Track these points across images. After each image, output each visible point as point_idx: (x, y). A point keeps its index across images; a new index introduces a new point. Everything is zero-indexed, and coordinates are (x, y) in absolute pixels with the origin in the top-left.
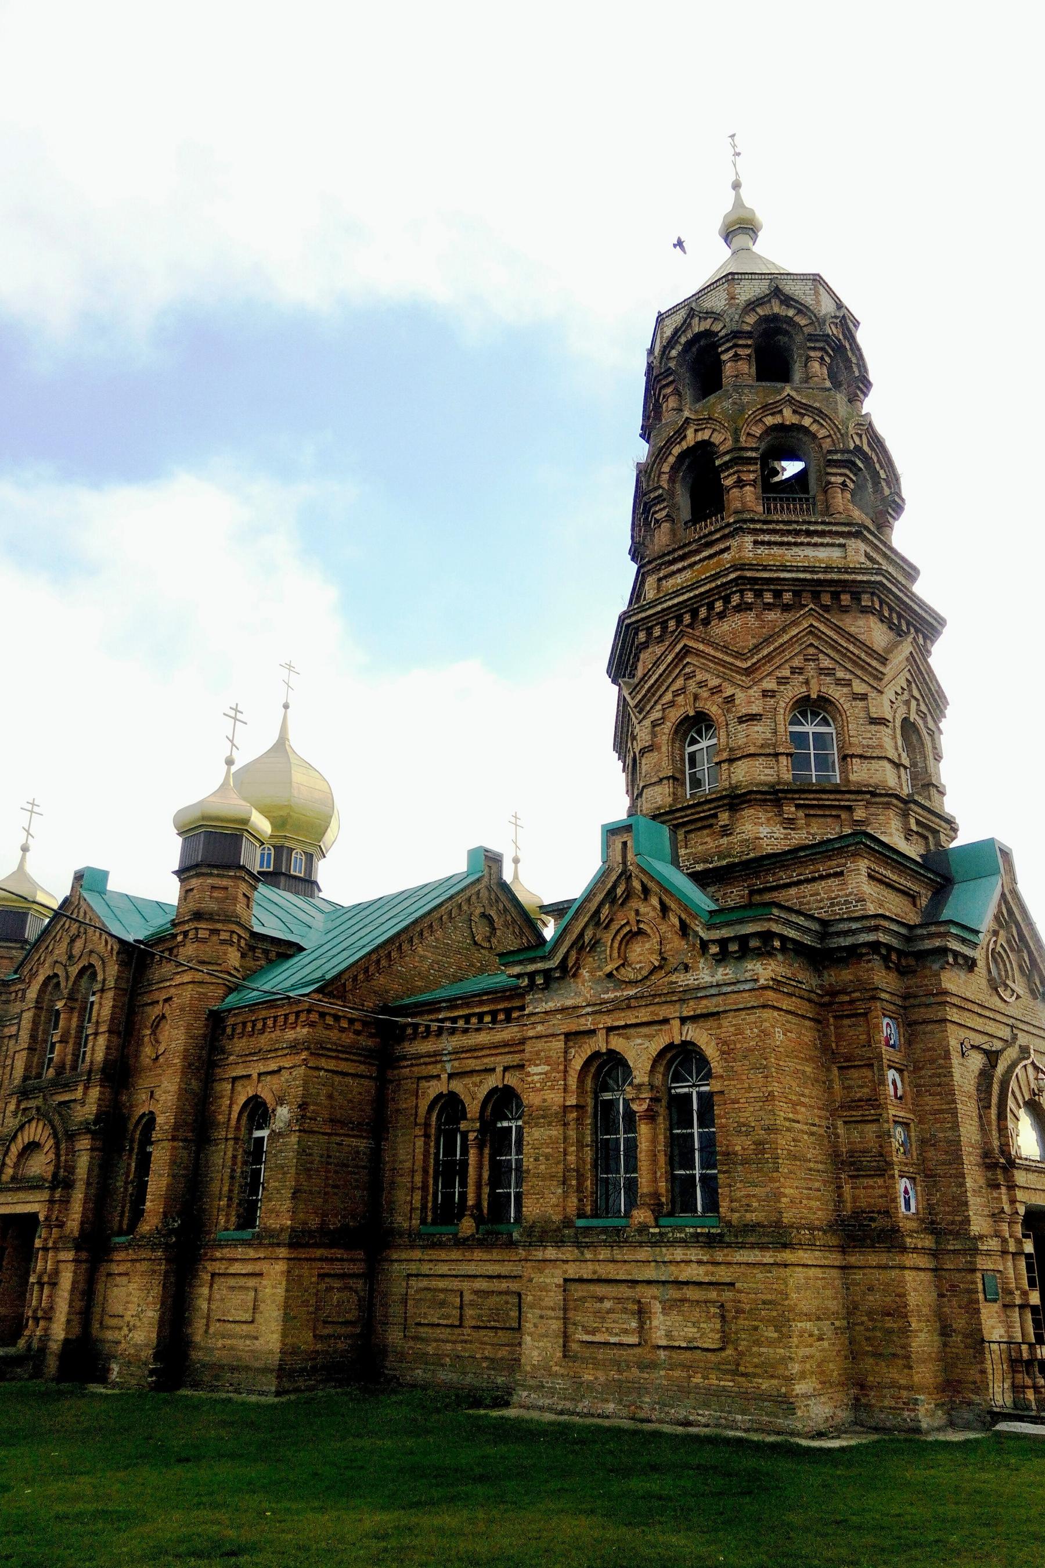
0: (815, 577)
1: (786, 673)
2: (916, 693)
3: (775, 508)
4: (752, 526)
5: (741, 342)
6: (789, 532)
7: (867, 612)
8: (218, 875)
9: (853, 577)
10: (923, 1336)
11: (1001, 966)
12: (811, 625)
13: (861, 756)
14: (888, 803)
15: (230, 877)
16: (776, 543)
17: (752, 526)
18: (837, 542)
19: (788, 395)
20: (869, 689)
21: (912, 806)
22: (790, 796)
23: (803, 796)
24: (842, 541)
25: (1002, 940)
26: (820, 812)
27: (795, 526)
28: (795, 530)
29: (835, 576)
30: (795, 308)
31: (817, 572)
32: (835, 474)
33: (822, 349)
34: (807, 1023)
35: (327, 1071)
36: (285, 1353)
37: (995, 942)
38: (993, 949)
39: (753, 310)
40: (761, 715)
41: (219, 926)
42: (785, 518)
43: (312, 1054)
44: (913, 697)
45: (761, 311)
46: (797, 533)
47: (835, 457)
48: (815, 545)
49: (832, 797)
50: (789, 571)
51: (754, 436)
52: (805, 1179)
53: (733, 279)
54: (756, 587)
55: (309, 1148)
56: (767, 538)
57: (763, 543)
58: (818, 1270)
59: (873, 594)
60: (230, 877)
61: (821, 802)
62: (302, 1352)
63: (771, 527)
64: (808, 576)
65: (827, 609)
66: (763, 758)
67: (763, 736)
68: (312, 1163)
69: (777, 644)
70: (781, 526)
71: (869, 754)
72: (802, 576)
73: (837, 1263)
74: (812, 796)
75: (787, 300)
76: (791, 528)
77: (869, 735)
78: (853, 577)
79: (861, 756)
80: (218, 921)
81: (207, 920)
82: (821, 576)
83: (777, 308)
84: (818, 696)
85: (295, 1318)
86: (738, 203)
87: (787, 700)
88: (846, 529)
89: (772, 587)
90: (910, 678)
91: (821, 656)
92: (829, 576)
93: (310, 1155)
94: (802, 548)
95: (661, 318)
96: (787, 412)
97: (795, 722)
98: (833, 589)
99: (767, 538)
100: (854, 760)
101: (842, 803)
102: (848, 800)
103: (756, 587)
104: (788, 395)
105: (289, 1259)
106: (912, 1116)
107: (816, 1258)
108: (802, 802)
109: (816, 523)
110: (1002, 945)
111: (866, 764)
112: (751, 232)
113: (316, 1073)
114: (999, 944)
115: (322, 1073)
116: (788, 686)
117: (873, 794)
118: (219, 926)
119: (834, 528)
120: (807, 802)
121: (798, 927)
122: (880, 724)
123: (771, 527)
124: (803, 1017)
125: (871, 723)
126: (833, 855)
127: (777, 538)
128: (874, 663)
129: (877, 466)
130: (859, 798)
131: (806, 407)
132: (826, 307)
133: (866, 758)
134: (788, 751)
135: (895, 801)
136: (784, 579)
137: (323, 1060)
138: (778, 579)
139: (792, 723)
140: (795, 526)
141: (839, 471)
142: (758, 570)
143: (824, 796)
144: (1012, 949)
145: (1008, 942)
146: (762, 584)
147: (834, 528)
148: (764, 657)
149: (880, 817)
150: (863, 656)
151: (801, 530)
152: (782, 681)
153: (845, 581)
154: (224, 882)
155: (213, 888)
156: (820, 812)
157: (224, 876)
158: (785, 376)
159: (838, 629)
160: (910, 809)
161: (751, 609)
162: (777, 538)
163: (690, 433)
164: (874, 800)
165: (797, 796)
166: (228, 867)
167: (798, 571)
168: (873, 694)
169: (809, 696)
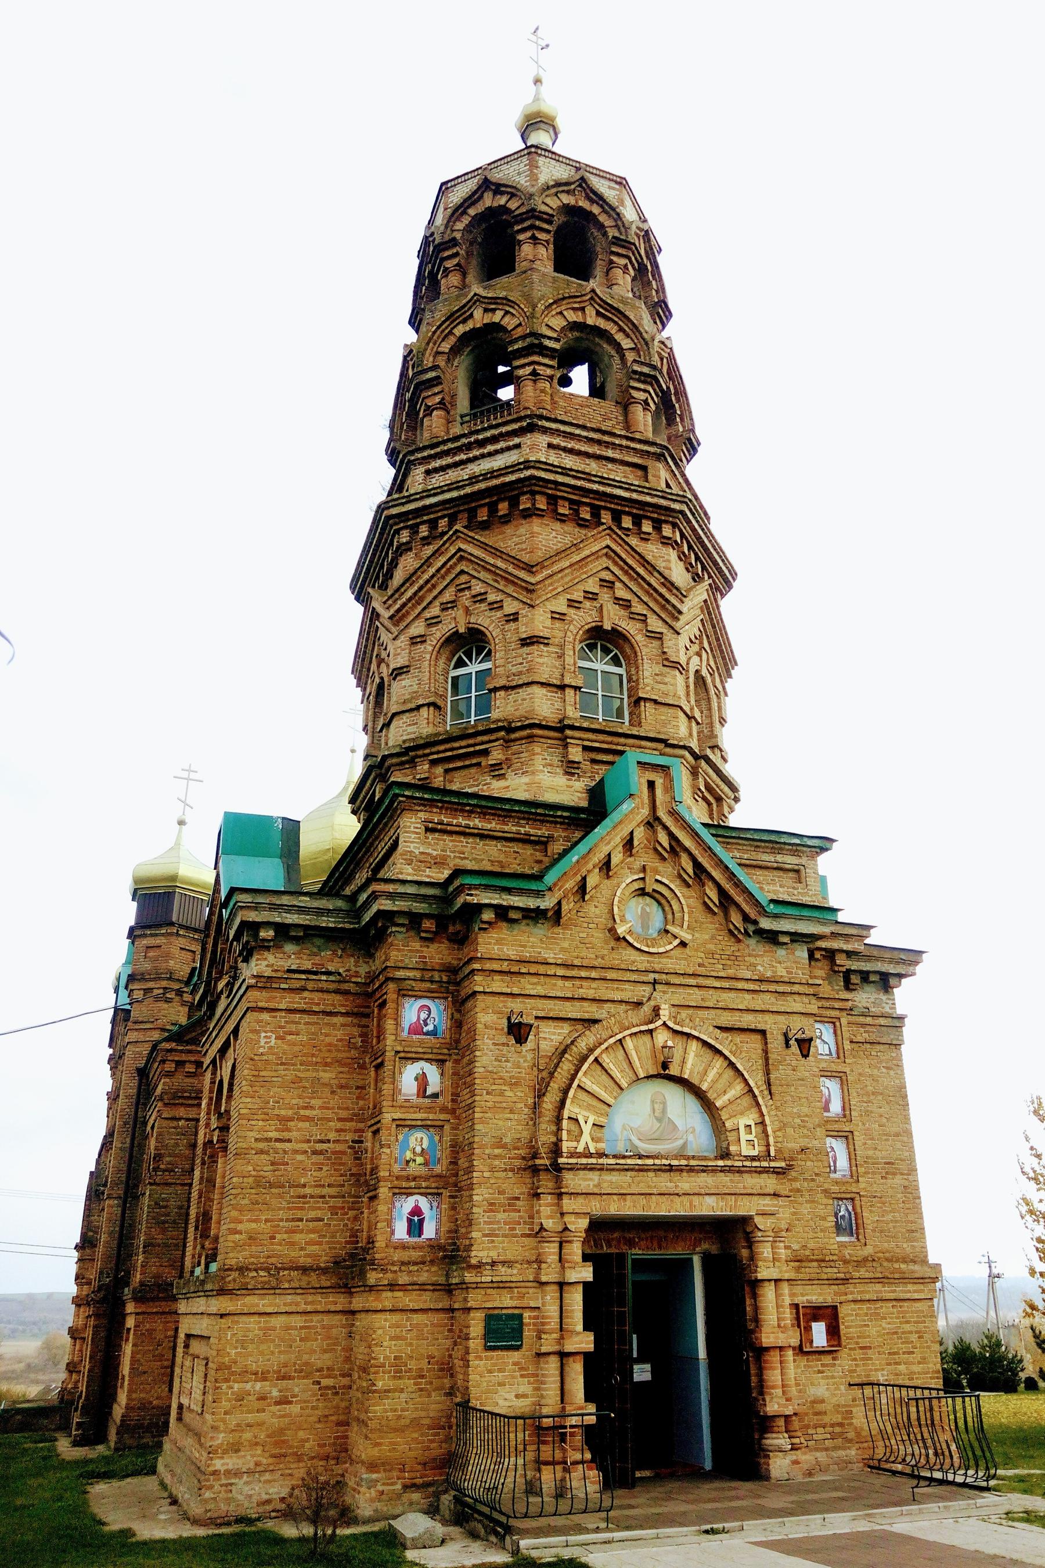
0: (462, 493)
1: (435, 610)
4: (419, 456)
5: (446, 254)
6: (459, 450)
7: (530, 516)
8: (152, 935)
9: (502, 480)
11: (667, 908)
12: (460, 550)
13: (505, 688)
14: (531, 737)
15: (163, 935)
16: (449, 466)
17: (419, 456)
18: (511, 443)
19: (475, 294)
20: (521, 606)
22: (420, 753)
23: (434, 750)
24: (517, 440)
26: (459, 764)
27: (465, 441)
28: (464, 445)
29: (482, 486)
30: (508, 193)
31: (463, 487)
32: (523, 366)
33: (532, 227)
34: (338, 1020)
35: (188, 1120)
40: (407, 667)
41: (151, 985)
43: (166, 1105)
45: (472, 212)
46: (469, 447)
47: (516, 347)
48: (490, 454)
49: (463, 743)
50: (435, 495)
51: (443, 353)
52: (289, 1209)
53: (447, 188)
54: (410, 523)
55: (163, 1200)
56: (437, 463)
57: (436, 470)
58: (298, 1318)
59: (533, 493)
60: (163, 935)
61: (455, 753)
62: (153, 1408)
63: (438, 450)
64: (455, 494)
65: (485, 526)
66: (407, 714)
67: (410, 690)
68: (168, 1215)
69: (421, 582)
70: (450, 445)
71: (514, 683)
72: (448, 496)
73: (339, 1307)
74: (442, 748)
75: (498, 188)
76: (459, 444)
77: (520, 660)
78: (502, 480)
79: (505, 688)
80: (151, 980)
81: (139, 980)
82: (468, 490)
83: (488, 201)
84: (469, 629)
85: (145, 1373)
86: (537, 99)
87: (434, 643)
88: (516, 426)
89: (425, 518)
92: (476, 487)
93: (165, 1207)
94: (477, 462)
96: (590, 311)
98: (487, 500)
99: (437, 463)
100: (498, 694)
101: (478, 748)
102: (483, 743)
103: (410, 523)
104: (475, 294)
105: (137, 1314)
106: (442, 1117)
107: (285, 1304)
108: (435, 756)
109: (484, 429)
111: (513, 695)
112: (542, 125)
113: (175, 1124)
115: (181, 1123)
116: (440, 625)
117: (510, 730)
118: (151, 985)
119: (504, 429)
120: (441, 755)
121: (301, 910)
122: (532, 644)
123: (438, 450)
125: (523, 645)
126: (803, 852)
127: (449, 460)
128: (522, 574)
130: (493, 738)
131: (494, 300)
133: (514, 688)
134: (427, 701)
136: (431, 506)
137: (182, 1109)
138: (425, 507)
140: (465, 441)
141: (526, 361)
142: (403, 504)
143: (456, 745)
146: (414, 518)
147: (504, 429)
148: (410, 600)
149: (522, 755)
150: (511, 569)
151: (470, 443)
152: (433, 622)
153: (496, 487)
154: (158, 941)
155: (149, 947)
156: (459, 764)
157: (156, 935)
158: (584, 274)
159: (484, 546)
160: (567, 737)
161: (410, 549)
162: (449, 460)
164: (513, 736)
165: (427, 751)
166: (159, 926)
167: (443, 492)
168: (524, 611)
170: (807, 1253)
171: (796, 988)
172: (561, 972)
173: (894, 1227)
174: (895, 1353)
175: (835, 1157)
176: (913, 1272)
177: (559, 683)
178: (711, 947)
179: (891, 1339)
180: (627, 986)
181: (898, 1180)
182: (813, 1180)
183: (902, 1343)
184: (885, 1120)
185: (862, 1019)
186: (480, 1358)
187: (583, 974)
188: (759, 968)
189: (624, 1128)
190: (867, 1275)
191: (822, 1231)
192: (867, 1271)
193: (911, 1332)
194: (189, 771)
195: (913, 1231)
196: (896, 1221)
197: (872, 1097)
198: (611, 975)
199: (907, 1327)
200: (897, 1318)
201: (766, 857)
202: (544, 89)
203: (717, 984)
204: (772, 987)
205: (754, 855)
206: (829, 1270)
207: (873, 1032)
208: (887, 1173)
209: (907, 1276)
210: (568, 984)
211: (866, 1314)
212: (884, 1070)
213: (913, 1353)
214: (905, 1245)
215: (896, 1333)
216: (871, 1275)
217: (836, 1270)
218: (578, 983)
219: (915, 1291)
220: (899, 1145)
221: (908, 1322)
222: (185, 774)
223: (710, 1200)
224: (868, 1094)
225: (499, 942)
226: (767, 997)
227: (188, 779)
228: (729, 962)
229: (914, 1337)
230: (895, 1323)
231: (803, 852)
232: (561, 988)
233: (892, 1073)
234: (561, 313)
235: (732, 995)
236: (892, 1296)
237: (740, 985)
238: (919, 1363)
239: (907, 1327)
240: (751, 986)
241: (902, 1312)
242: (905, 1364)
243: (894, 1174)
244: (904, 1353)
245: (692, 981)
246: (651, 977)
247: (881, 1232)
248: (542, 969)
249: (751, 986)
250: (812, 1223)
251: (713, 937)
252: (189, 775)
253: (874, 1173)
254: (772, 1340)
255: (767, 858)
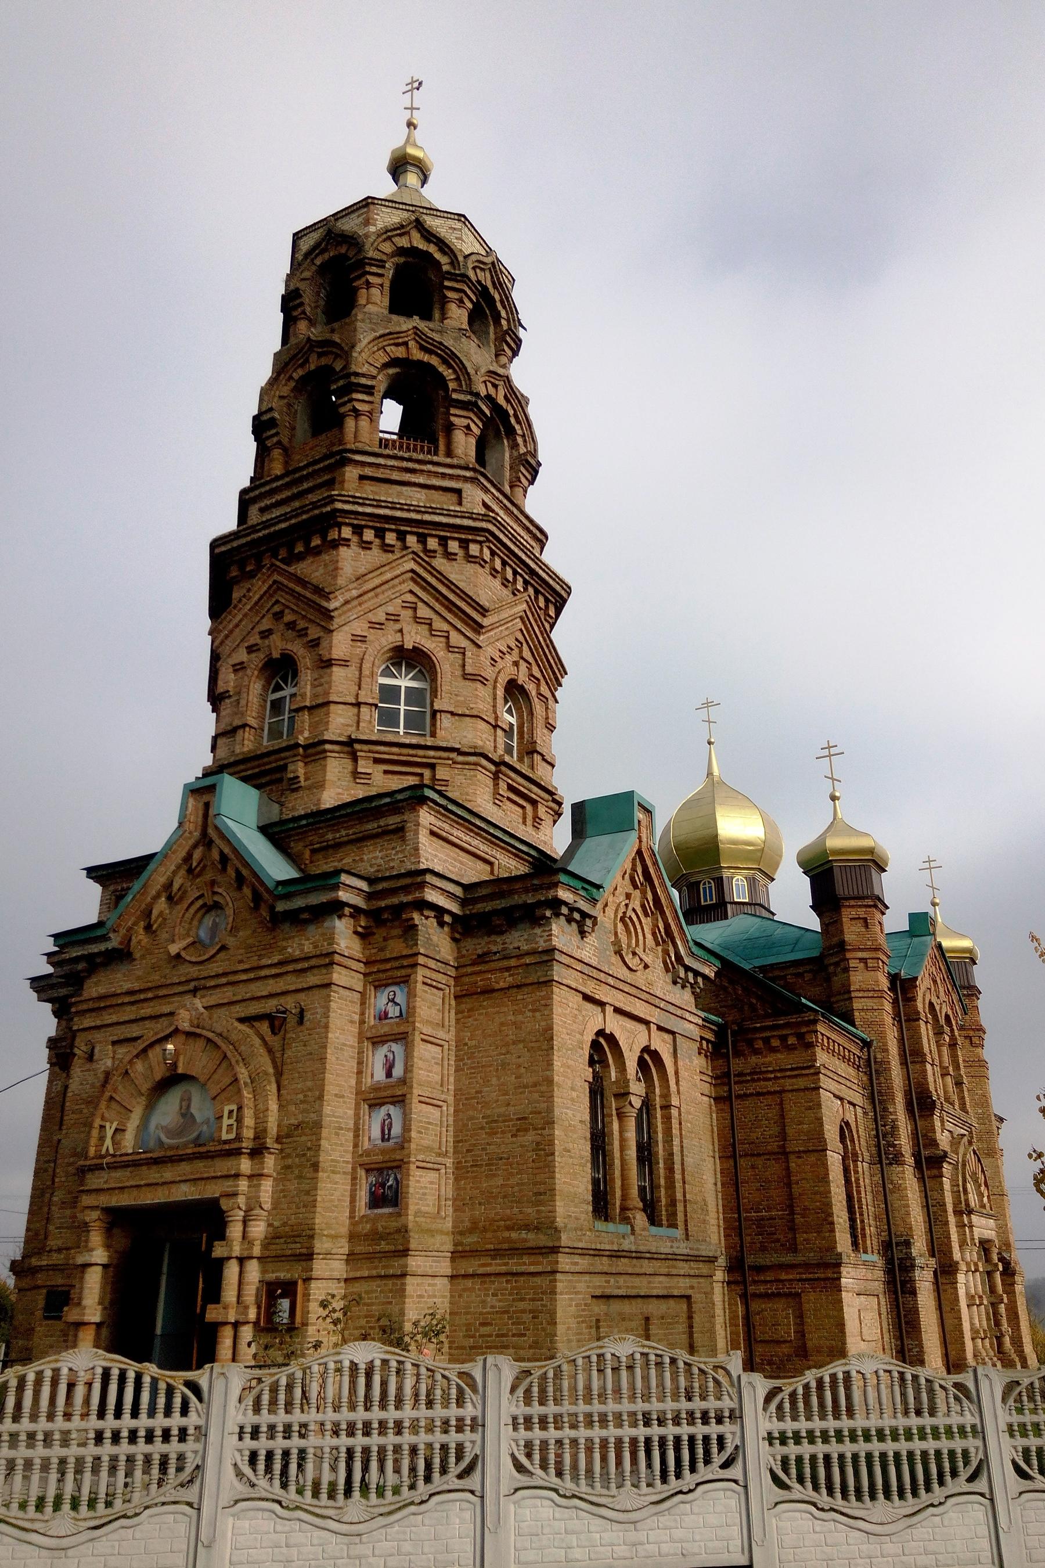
1: (381, 616)
2: (527, 654)
3: (422, 447)
10: (254, 1273)
21: (503, 768)
25: (636, 903)
36: (461, 1233)
37: (627, 905)
38: (624, 913)
39: (389, 238)
42: (421, 457)
44: (522, 658)
75: (429, 235)
90: (521, 638)
91: (420, 604)
95: (297, 237)
97: (387, 673)
110: (634, 910)
114: (630, 907)
124: (359, 961)
126: (403, 807)
129: (513, 420)
132: (466, 245)
135: (484, 762)
139: (384, 674)
144: (646, 915)
145: (643, 906)
163: (313, 358)
169: (403, 646)
170: (287, 1229)
171: (313, 962)
172: (127, 999)
173: (520, 1191)
174: (503, 1335)
175: (391, 1124)
176: (525, 1240)
177: (354, 701)
178: (250, 941)
179: (500, 1319)
180: (176, 999)
181: (530, 1137)
182: (304, 1155)
183: (513, 1324)
184: (523, 1070)
185: (505, 963)
186: (41, 1325)
187: (142, 996)
188: (290, 950)
189: (157, 1127)
190: (387, 1248)
191: (304, 1206)
192: (388, 1244)
193: (523, 1311)
194: (829, 747)
195: (540, 1194)
196: (522, 1184)
197: (511, 1047)
198: (161, 992)
199: (522, 1305)
200: (510, 1294)
201: (369, 826)
202: (417, 134)
203: (244, 977)
204: (290, 968)
205: (358, 828)
206: (293, 1246)
207: (518, 974)
208: (518, 1130)
209: (517, 1246)
210: (134, 1008)
211: (391, 1291)
212: (529, 1014)
213: (524, 1335)
214: (530, 1210)
215: (507, 1312)
216: (392, 1248)
217: (298, 1245)
218: (140, 1005)
219: (531, 1264)
220: (536, 1096)
221: (522, 1300)
222: (826, 752)
223: (184, 1187)
224: (507, 1045)
225: (96, 984)
226: (289, 978)
227: (830, 756)
228: (263, 952)
229: (527, 1317)
230: (507, 1300)
231: (403, 807)
232: (129, 1013)
233: (538, 1014)
234: (383, 348)
235: (259, 984)
236: (503, 1269)
237: (263, 973)
238: (530, 1347)
239: (522, 1305)
240: (274, 971)
241: (516, 1288)
242: (514, 1348)
243: (526, 1130)
244: (514, 1335)
245: (224, 980)
246: (192, 985)
247: (505, 1197)
248: (114, 1001)
249: (274, 971)
250: (297, 1199)
251: (254, 931)
252: (830, 752)
253: (503, 1132)
254: (214, 1316)
255: (371, 826)
